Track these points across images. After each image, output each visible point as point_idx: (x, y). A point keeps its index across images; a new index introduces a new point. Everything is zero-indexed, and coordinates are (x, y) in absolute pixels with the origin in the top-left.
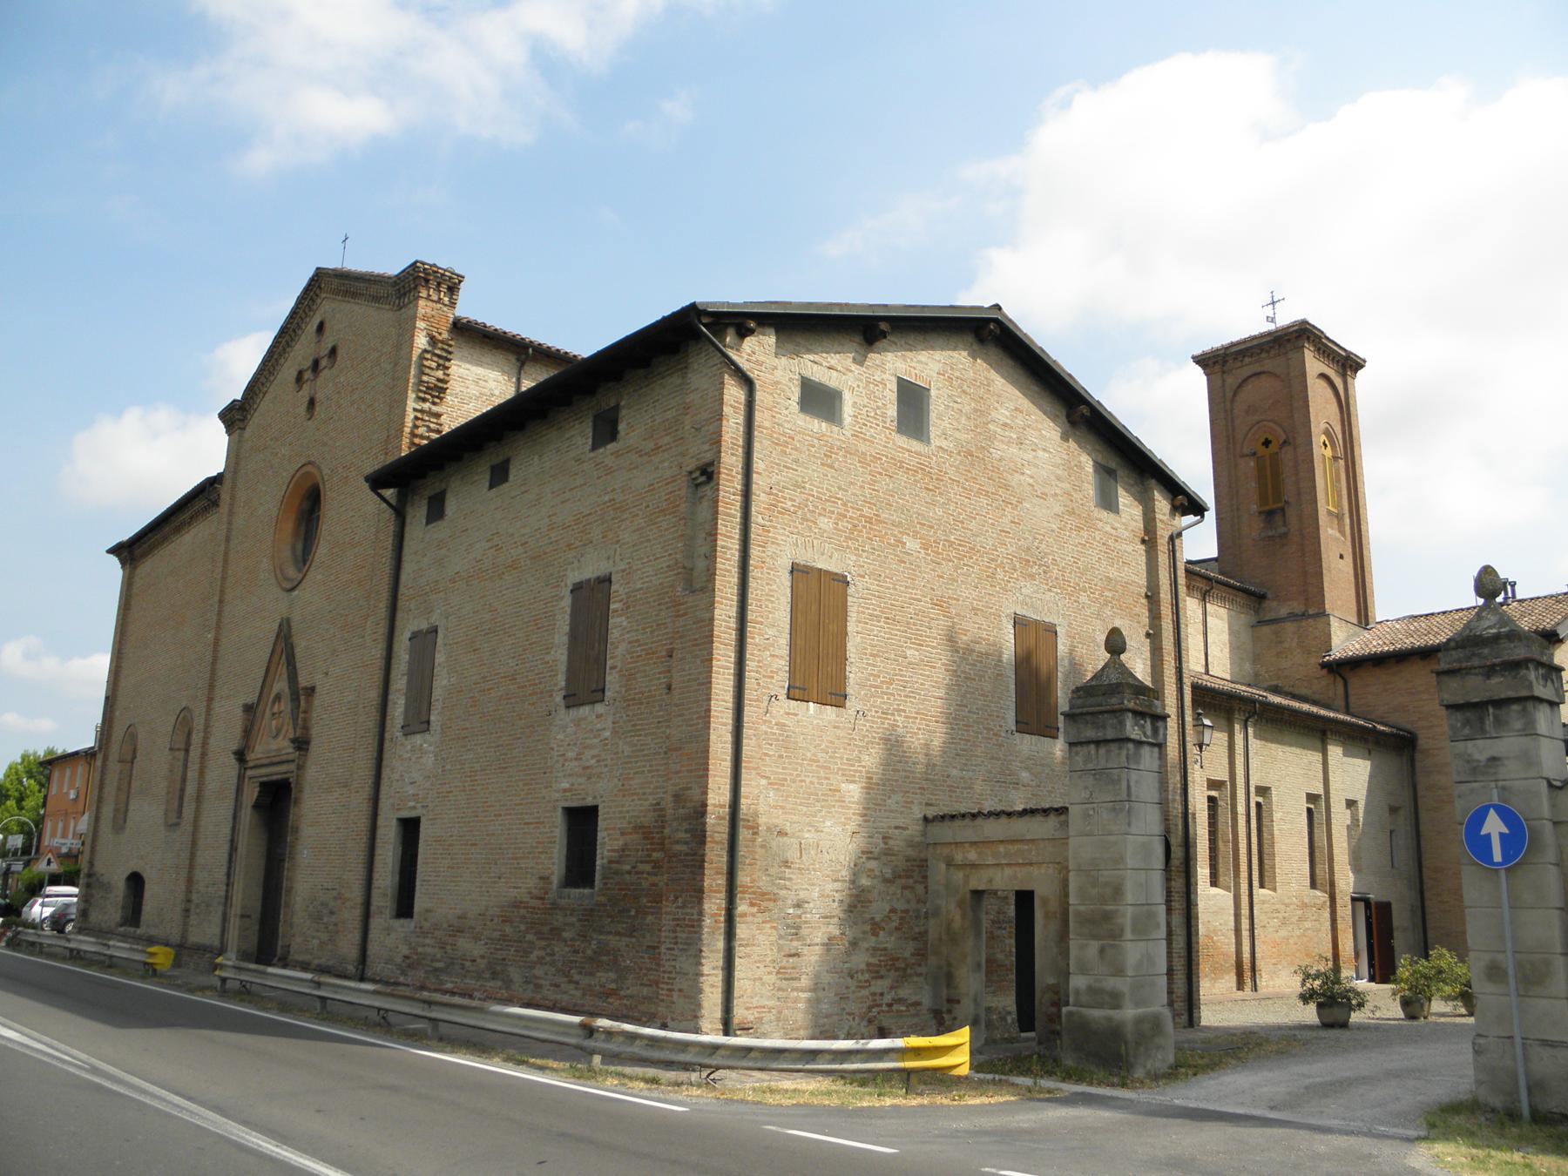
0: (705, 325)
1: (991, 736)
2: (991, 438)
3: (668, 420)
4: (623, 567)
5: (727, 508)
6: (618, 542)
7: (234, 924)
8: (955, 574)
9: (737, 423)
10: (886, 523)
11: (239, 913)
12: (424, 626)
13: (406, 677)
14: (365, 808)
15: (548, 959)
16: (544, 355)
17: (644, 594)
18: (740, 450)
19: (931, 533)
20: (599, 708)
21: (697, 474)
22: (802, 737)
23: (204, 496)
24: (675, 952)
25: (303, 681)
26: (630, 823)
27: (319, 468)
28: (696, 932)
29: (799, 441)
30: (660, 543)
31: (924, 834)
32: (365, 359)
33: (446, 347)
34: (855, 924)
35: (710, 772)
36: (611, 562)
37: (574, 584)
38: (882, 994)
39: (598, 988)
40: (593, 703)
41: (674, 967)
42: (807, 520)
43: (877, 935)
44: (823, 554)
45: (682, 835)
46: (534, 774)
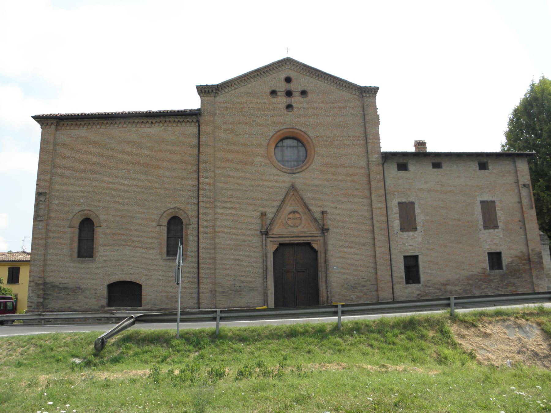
45: (535, 258)
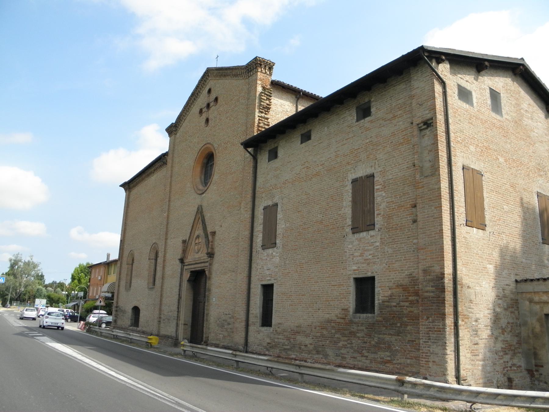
0: (426, 56)
1: (534, 245)
2: (522, 116)
3: (400, 104)
4: (380, 170)
5: (441, 138)
6: (376, 159)
7: (181, 328)
8: (516, 173)
9: (440, 101)
10: (492, 150)
11: (183, 323)
12: (270, 203)
13: (262, 225)
14: (246, 280)
15: (349, 346)
16: (307, 96)
17: (394, 180)
18: (443, 113)
19: (507, 155)
20: (372, 233)
21: (422, 124)
22: (472, 243)
23: (161, 161)
24: (430, 343)
25: (209, 230)
26: (394, 284)
27: (212, 145)
28: (442, 334)
29: (460, 112)
30: (401, 157)
31: (516, 288)
32: (232, 100)
33: (270, 91)
34: (496, 329)
35: (445, 259)
36: (373, 168)
37: (353, 180)
38: (508, 362)
39: (379, 359)
40: (368, 231)
41: (429, 351)
42: (466, 147)
43: (503, 334)
44: (472, 162)
46: (336, 264)
